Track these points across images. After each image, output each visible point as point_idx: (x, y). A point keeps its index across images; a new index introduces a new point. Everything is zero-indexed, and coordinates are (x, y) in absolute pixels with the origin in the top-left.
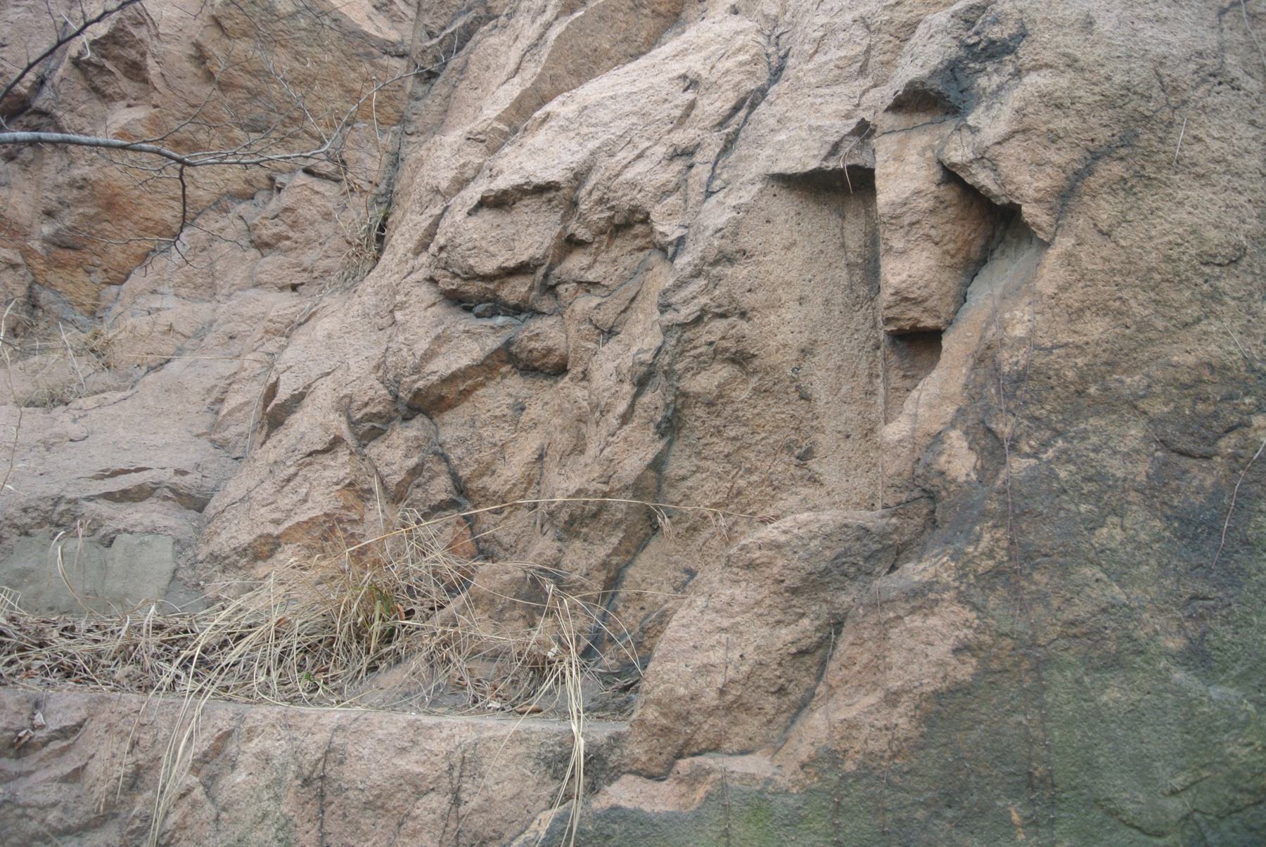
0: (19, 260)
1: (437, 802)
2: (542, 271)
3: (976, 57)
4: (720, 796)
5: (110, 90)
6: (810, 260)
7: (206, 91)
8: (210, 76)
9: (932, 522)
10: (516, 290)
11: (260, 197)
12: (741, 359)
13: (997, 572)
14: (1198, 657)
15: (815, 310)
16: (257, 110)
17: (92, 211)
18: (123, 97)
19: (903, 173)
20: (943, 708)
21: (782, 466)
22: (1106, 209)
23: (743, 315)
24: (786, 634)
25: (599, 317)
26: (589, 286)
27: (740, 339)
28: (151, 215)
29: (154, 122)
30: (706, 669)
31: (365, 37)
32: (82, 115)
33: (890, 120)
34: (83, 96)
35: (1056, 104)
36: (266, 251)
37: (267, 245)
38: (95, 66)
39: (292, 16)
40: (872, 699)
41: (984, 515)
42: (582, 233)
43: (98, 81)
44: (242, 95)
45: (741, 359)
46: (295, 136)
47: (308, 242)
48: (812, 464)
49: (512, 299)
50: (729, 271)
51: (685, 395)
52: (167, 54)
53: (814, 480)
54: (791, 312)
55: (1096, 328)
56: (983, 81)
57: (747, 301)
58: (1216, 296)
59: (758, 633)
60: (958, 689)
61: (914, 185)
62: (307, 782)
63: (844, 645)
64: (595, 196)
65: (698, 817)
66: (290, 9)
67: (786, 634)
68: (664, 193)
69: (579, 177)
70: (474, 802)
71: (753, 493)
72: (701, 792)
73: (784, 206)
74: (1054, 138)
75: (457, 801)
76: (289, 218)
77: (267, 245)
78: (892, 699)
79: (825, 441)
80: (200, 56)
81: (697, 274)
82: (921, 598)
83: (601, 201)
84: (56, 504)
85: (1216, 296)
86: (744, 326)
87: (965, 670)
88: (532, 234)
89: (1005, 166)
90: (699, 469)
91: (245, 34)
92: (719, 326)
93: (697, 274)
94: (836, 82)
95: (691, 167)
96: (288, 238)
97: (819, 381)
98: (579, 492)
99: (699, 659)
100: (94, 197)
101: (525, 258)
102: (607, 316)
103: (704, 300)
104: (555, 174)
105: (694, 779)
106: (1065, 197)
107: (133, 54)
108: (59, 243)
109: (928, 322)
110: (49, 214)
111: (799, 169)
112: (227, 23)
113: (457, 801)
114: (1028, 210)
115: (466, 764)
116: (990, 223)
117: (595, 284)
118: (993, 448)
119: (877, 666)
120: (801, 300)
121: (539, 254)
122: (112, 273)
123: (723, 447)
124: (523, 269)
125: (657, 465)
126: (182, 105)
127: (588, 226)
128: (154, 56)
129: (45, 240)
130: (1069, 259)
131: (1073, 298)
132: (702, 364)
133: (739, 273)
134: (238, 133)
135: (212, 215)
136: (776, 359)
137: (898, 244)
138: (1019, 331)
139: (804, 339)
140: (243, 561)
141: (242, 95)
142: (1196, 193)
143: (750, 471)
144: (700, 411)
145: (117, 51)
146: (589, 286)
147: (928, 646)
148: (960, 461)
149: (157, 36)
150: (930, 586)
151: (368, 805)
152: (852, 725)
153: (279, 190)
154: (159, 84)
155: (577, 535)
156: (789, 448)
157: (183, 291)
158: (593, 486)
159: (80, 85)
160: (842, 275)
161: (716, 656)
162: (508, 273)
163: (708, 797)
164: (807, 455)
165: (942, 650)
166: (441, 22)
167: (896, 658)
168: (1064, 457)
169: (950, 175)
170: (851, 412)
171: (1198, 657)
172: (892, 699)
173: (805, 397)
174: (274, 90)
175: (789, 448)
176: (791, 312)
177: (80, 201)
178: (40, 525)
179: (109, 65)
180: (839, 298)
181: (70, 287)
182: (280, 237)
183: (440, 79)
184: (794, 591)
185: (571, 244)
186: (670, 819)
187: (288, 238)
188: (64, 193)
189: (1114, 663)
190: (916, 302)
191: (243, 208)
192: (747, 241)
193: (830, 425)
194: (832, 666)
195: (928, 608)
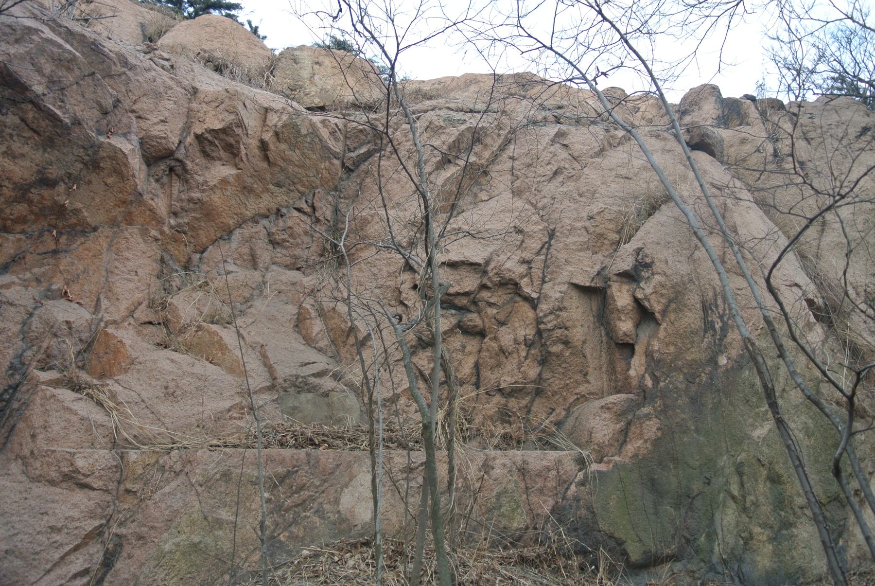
0: (159, 237)
1: (554, 472)
2: (473, 296)
3: (641, 266)
4: (616, 465)
5: (214, 154)
6: (583, 313)
7: (265, 165)
8: (266, 158)
9: (645, 398)
10: (464, 301)
11: (272, 218)
12: (566, 343)
13: (661, 411)
14: (697, 431)
15: (586, 329)
16: (281, 177)
17: (198, 216)
18: (220, 159)
19: (621, 296)
20: (656, 443)
21: (579, 377)
22: (672, 316)
23: (566, 329)
24: (618, 426)
25: (498, 317)
26: (491, 305)
27: (567, 336)
28: (225, 221)
29: (238, 177)
30: (605, 435)
31: (329, 149)
32: (197, 165)
33: (615, 278)
34: (198, 154)
35: (663, 286)
36: (276, 246)
37: (278, 244)
38: (209, 141)
39: (305, 136)
40: (641, 441)
41: (657, 396)
42: (489, 284)
43: (208, 149)
44: (278, 169)
45: (566, 343)
46: (292, 191)
47: (298, 244)
48: (588, 377)
49: (459, 304)
50: (561, 313)
51: (550, 353)
52: (249, 145)
53: (588, 382)
54: (579, 329)
55: (672, 349)
56: (643, 273)
57: (568, 324)
58: (693, 342)
59: (612, 426)
60: (659, 439)
61: (628, 302)
62: (519, 470)
63: (633, 428)
64: (495, 271)
65: (612, 471)
66: (306, 132)
67: (618, 426)
68: (522, 277)
69: (487, 263)
70: (562, 472)
71: (571, 385)
72: (611, 465)
73: (574, 294)
74: (662, 295)
75: (558, 472)
76: (289, 232)
77: (278, 244)
78: (646, 441)
79: (590, 370)
80: (264, 146)
81: (551, 313)
82: (648, 417)
83: (497, 274)
84: (297, 379)
85: (693, 342)
86: (566, 332)
87: (659, 434)
88: (469, 282)
89: (652, 301)
90: (553, 377)
91: (286, 141)
92: (559, 331)
93: (551, 313)
94: (580, 250)
95: (531, 268)
96: (288, 241)
97: (588, 352)
98: (515, 383)
99: (603, 433)
100: (202, 209)
101: (467, 290)
102: (501, 317)
103: (555, 322)
104: (479, 260)
105: (609, 462)
106: (664, 312)
107: (232, 140)
108: (179, 230)
109: (631, 342)
110: (175, 214)
111: (582, 284)
112: (281, 136)
113: (558, 472)
114: (657, 314)
115: (559, 462)
116: (644, 314)
117: (494, 304)
118: (656, 380)
119: (641, 434)
120: (582, 326)
121: (473, 289)
122: (198, 247)
123: (561, 370)
124: (466, 294)
125: (540, 375)
126: (252, 170)
127: (492, 282)
128: (244, 144)
129: (172, 227)
130: (666, 329)
131: (667, 340)
132: (554, 343)
133: (564, 314)
134: (271, 186)
135: (250, 224)
136: (577, 344)
137: (623, 318)
138: (656, 348)
139: (583, 338)
140: (388, 404)
141: (278, 169)
142: (689, 314)
143: (570, 378)
144: (554, 358)
145: (223, 136)
146: (491, 305)
147: (651, 428)
148: (649, 382)
149: (247, 134)
150: (649, 414)
151: (537, 475)
152: (639, 447)
153: (282, 216)
154: (244, 159)
155: (513, 396)
156: (581, 372)
157: (238, 262)
158: (520, 381)
159: (196, 148)
160: (592, 318)
161: (606, 432)
162: (458, 294)
163: (614, 466)
164: (586, 375)
165: (654, 429)
166: (355, 145)
167: (645, 431)
168: (670, 382)
169: (636, 301)
170: (596, 362)
171: (697, 431)
172: (646, 441)
173: (585, 357)
174: (290, 168)
175: (581, 372)
176: (579, 329)
177: (194, 210)
178: (290, 387)
179: (217, 142)
180: (592, 326)
181: (176, 252)
182: (284, 240)
183: (355, 174)
184: (619, 415)
185: (484, 287)
186: (608, 471)
187: (288, 241)
188: (184, 204)
189: (684, 432)
190: (628, 336)
191: (265, 222)
192: (566, 304)
193: (592, 365)
194: (630, 434)
195: (650, 419)
